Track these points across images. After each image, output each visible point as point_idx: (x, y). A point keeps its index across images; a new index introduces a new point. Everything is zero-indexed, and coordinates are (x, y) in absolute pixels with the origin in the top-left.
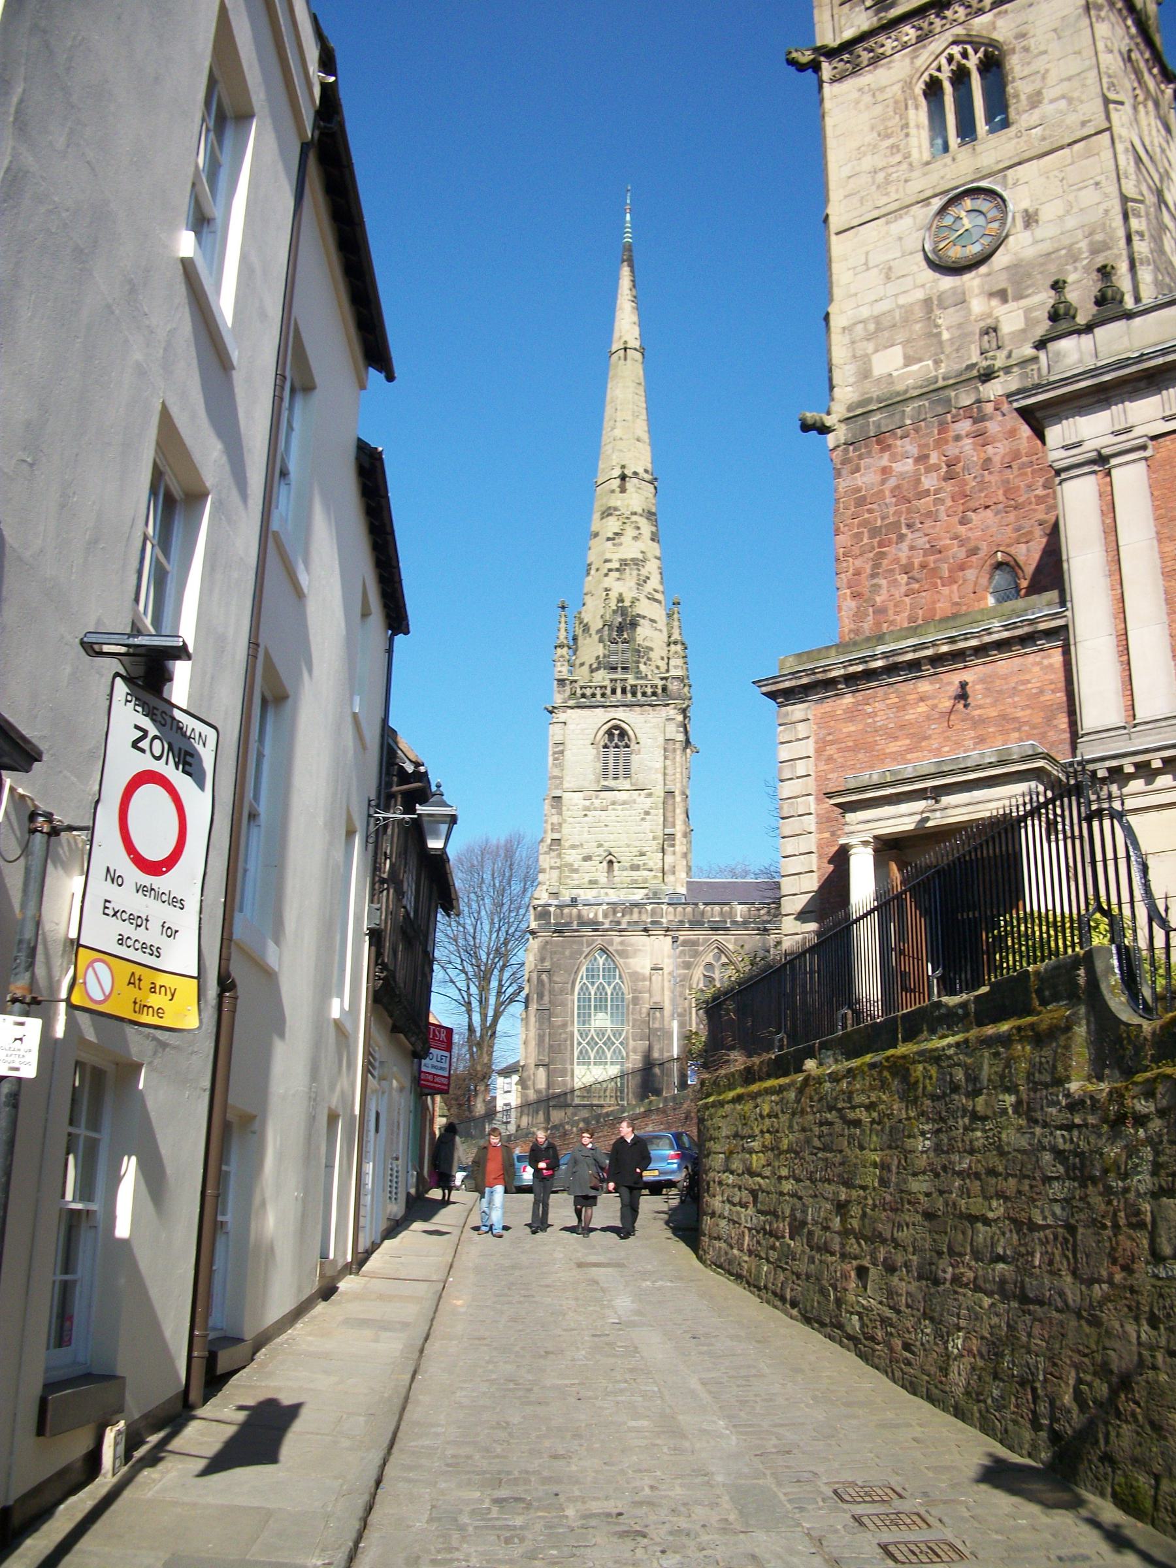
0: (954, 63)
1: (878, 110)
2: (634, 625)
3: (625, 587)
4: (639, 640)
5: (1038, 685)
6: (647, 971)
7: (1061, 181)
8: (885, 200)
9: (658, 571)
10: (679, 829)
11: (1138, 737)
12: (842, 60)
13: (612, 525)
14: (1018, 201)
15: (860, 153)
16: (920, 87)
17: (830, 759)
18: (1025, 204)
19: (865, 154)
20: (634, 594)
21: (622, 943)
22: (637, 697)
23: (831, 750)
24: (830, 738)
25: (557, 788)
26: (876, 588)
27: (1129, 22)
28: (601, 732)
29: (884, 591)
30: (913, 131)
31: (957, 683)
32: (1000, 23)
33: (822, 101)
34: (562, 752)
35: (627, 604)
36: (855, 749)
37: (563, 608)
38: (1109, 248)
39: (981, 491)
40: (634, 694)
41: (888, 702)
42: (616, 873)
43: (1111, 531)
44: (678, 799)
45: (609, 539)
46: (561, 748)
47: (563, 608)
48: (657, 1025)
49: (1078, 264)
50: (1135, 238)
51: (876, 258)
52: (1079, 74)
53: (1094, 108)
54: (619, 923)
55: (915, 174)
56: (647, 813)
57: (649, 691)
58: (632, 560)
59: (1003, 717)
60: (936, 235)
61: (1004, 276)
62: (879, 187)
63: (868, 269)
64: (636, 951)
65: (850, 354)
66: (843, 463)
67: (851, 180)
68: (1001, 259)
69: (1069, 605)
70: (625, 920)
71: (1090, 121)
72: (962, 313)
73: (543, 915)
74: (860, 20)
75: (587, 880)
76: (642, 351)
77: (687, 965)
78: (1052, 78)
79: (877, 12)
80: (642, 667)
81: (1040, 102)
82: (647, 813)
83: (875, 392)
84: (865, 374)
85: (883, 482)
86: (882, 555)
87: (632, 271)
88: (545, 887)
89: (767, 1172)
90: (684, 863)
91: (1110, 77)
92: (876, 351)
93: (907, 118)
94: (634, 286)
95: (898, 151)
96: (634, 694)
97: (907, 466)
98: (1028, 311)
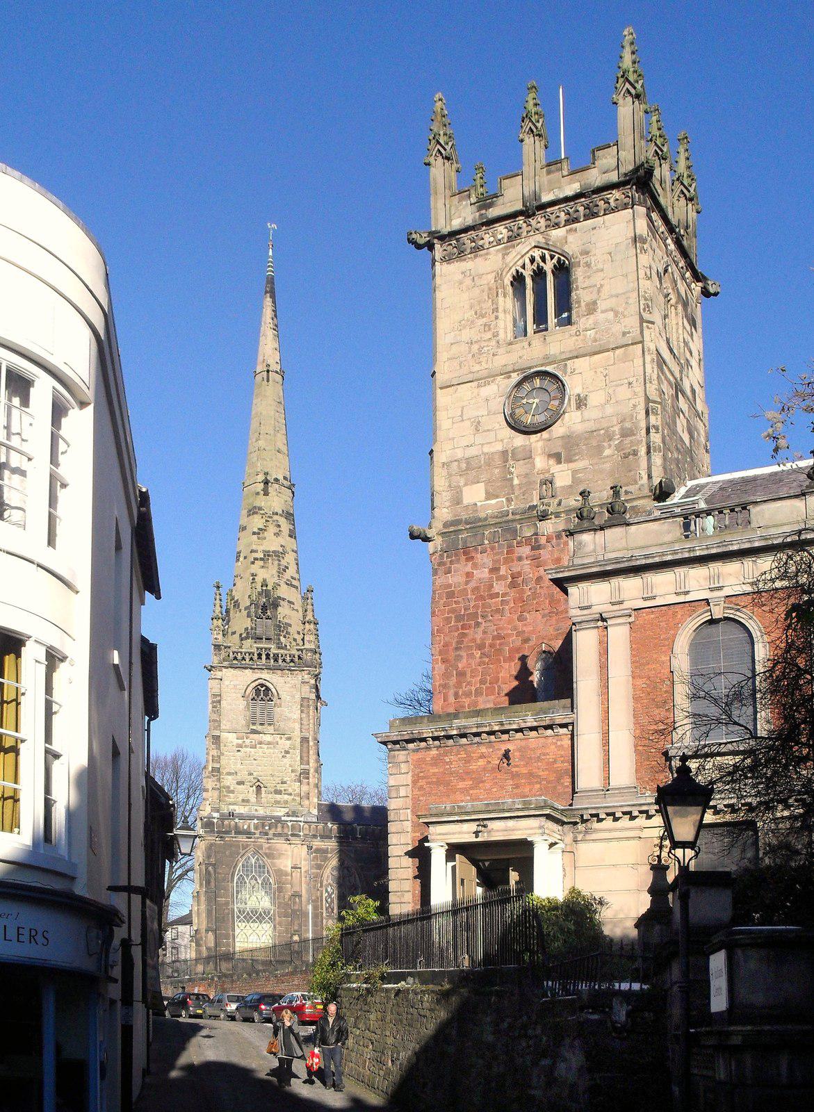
0: (535, 264)
1: (477, 291)
2: (275, 605)
3: (267, 574)
4: (280, 617)
5: (554, 757)
6: (289, 870)
7: (605, 377)
8: (477, 368)
9: (294, 562)
10: (312, 764)
11: (609, 797)
12: (451, 244)
13: (257, 522)
14: (574, 386)
15: (461, 326)
16: (508, 279)
17: (421, 788)
18: (578, 390)
19: (465, 328)
20: (275, 580)
21: (269, 848)
22: (276, 662)
23: (422, 783)
24: (422, 774)
25: (215, 728)
26: (459, 658)
27: (669, 241)
28: (250, 688)
29: (465, 660)
30: (501, 315)
31: (503, 749)
32: (571, 238)
33: (434, 276)
34: (219, 702)
35: (270, 588)
36: (438, 783)
37: (218, 587)
38: (634, 435)
39: (534, 599)
40: (276, 660)
41: (459, 756)
42: (263, 795)
43: (604, 667)
44: (311, 743)
45: (254, 533)
46: (218, 698)
47: (218, 587)
48: (296, 907)
49: (611, 443)
50: (652, 431)
51: (470, 413)
52: (624, 293)
53: (632, 323)
54: (266, 834)
55: (501, 351)
56: (287, 752)
57: (288, 659)
58: (274, 552)
59: (531, 774)
60: (513, 403)
61: (560, 442)
62: (473, 356)
63: (463, 420)
64: (280, 855)
65: (447, 484)
66: (439, 564)
67: (454, 346)
68: (558, 430)
69: (575, 711)
70: (271, 832)
71: (629, 333)
72: (529, 466)
73: (208, 825)
74: (464, 214)
75: (240, 799)
76: (282, 373)
77: (319, 867)
78: (605, 292)
79: (480, 209)
80: (282, 639)
81: (595, 310)
82: (287, 752)
83: (464, 516)
84: (457, 500)
85: (467, 583)
86: (464, 635)
87: (274, 302)
88: (208, 802)
89: (379, 1032)
90: (316, 791)
91: (646, 299)
92: (466, 485)
93: (497, 304)
94: (276, 316)
95: (490, 329)
96: (276, 660)
97: (483, 574)
98: (575, 472)
